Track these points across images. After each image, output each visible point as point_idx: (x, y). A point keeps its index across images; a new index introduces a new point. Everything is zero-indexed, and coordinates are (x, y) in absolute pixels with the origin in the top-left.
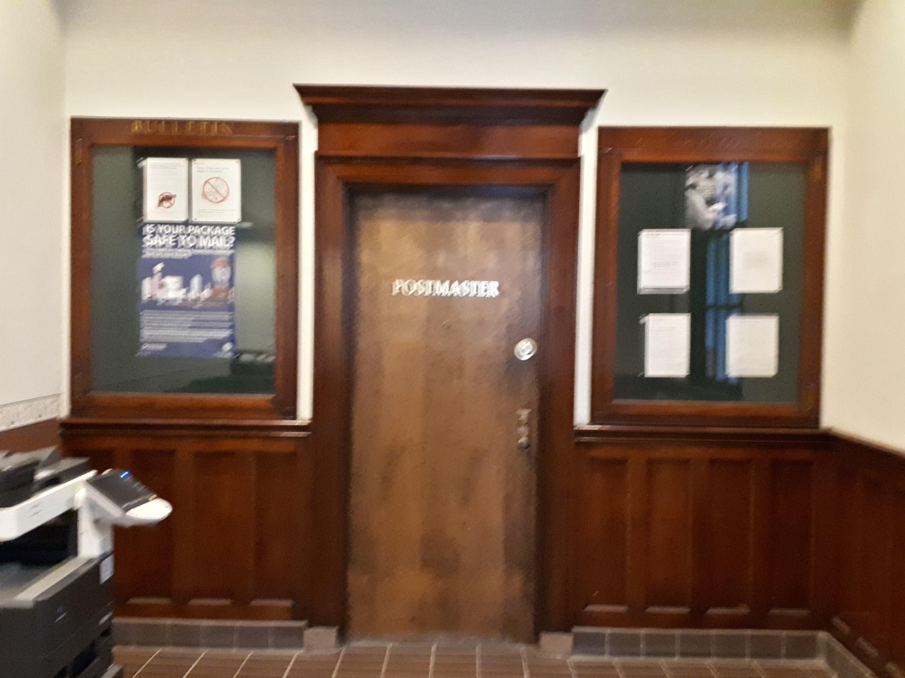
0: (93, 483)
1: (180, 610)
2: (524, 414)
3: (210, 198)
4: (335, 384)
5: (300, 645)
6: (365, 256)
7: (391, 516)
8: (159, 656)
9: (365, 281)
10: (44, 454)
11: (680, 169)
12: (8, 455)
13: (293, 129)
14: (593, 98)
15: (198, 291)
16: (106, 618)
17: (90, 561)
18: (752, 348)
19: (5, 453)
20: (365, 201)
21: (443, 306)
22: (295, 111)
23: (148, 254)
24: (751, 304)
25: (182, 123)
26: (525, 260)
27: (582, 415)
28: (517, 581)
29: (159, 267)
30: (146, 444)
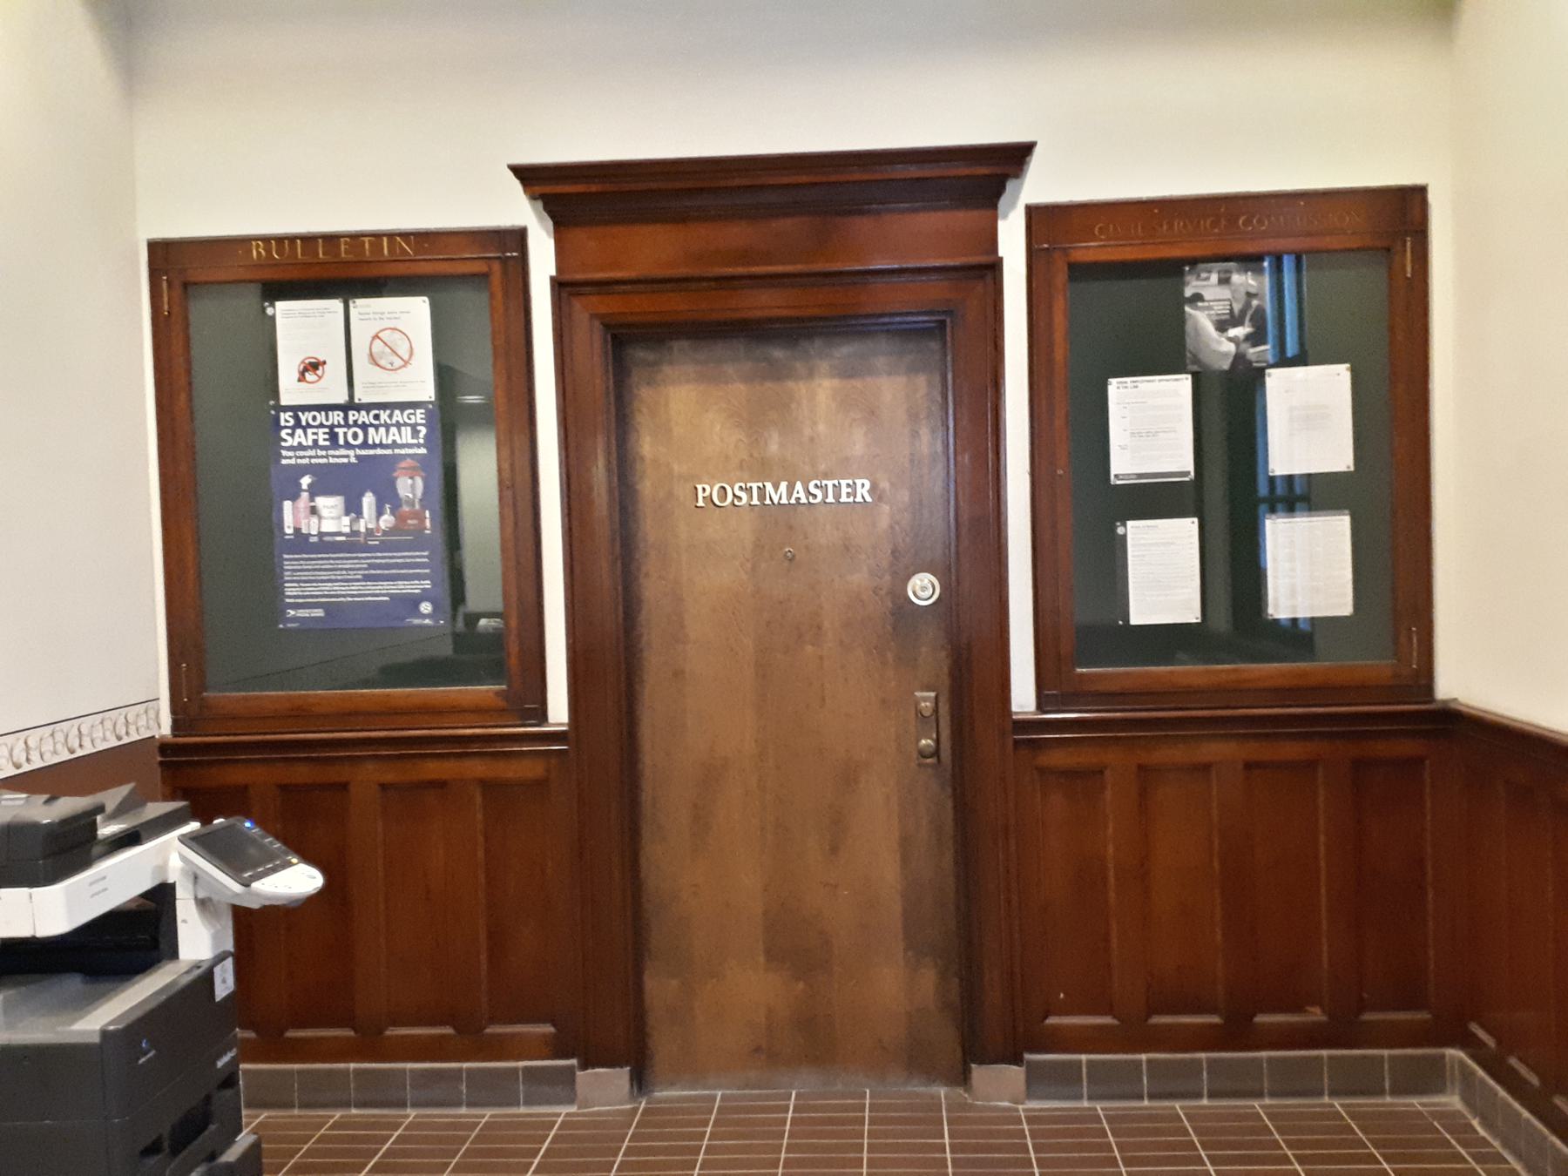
0: (191, 840)
3: (382, 363)
4: (608, 661)
5: (571, 1101)
6: (647, 446)
7: (708, 875)
9: (647, 486)
10: (112, 797)
11: (1174, 270)
12: (47, 802)
13: (518, 237)
14: (1014, 157)
16: (226, 1059)
17: (197, 966)
18: (1309, 567)
19: (45, 797)
20: (640, 354)
21: (779, 523)
22: (516, 209)
24: (1304, 495)
26: (915, 434)
27: (1023, 697)
28: (928, 978)
29: (306, 481)
30: (301, 774)
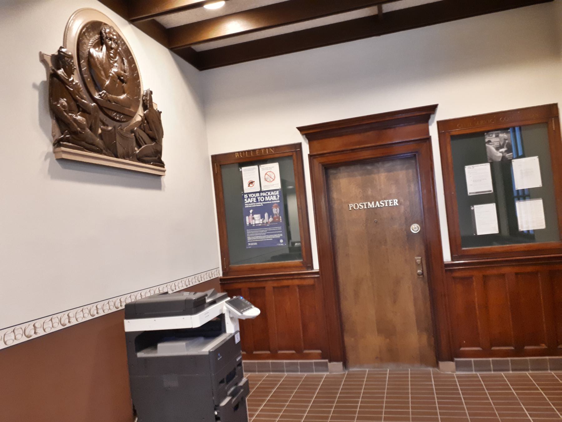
0: (229, 302)
1: (274, 356)
2: (418, 259)
5: (327, 370)
6: (335, 195)
7: (360, 310)
8: (267, 377)
9: (336, 206)
10: (209, 292)
11: (482, 134)
13: (299, 145)
14: (432, 109)
15: (268, 219)
20: (332, 171)
22: (299, 138)
23: (247, 206)
25: (254, 151)
27: (447, 257)
28: (425, 338)
29: (251, 211)
30: (254, 285)
